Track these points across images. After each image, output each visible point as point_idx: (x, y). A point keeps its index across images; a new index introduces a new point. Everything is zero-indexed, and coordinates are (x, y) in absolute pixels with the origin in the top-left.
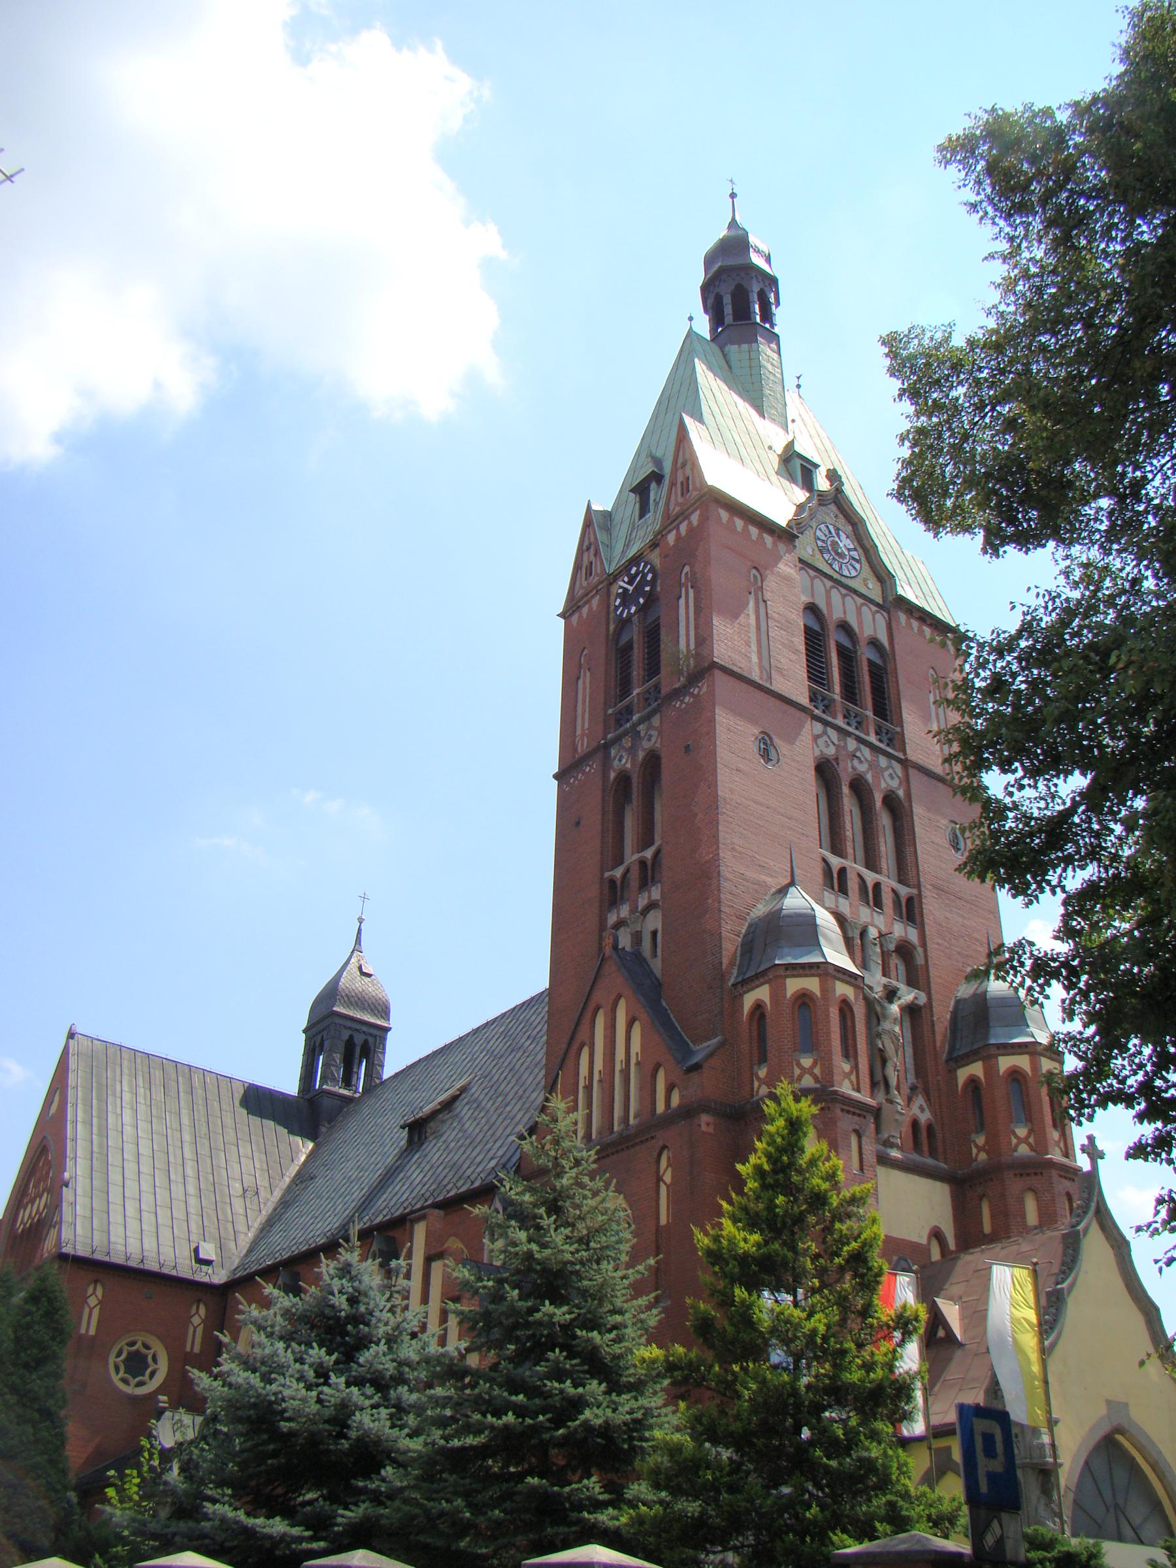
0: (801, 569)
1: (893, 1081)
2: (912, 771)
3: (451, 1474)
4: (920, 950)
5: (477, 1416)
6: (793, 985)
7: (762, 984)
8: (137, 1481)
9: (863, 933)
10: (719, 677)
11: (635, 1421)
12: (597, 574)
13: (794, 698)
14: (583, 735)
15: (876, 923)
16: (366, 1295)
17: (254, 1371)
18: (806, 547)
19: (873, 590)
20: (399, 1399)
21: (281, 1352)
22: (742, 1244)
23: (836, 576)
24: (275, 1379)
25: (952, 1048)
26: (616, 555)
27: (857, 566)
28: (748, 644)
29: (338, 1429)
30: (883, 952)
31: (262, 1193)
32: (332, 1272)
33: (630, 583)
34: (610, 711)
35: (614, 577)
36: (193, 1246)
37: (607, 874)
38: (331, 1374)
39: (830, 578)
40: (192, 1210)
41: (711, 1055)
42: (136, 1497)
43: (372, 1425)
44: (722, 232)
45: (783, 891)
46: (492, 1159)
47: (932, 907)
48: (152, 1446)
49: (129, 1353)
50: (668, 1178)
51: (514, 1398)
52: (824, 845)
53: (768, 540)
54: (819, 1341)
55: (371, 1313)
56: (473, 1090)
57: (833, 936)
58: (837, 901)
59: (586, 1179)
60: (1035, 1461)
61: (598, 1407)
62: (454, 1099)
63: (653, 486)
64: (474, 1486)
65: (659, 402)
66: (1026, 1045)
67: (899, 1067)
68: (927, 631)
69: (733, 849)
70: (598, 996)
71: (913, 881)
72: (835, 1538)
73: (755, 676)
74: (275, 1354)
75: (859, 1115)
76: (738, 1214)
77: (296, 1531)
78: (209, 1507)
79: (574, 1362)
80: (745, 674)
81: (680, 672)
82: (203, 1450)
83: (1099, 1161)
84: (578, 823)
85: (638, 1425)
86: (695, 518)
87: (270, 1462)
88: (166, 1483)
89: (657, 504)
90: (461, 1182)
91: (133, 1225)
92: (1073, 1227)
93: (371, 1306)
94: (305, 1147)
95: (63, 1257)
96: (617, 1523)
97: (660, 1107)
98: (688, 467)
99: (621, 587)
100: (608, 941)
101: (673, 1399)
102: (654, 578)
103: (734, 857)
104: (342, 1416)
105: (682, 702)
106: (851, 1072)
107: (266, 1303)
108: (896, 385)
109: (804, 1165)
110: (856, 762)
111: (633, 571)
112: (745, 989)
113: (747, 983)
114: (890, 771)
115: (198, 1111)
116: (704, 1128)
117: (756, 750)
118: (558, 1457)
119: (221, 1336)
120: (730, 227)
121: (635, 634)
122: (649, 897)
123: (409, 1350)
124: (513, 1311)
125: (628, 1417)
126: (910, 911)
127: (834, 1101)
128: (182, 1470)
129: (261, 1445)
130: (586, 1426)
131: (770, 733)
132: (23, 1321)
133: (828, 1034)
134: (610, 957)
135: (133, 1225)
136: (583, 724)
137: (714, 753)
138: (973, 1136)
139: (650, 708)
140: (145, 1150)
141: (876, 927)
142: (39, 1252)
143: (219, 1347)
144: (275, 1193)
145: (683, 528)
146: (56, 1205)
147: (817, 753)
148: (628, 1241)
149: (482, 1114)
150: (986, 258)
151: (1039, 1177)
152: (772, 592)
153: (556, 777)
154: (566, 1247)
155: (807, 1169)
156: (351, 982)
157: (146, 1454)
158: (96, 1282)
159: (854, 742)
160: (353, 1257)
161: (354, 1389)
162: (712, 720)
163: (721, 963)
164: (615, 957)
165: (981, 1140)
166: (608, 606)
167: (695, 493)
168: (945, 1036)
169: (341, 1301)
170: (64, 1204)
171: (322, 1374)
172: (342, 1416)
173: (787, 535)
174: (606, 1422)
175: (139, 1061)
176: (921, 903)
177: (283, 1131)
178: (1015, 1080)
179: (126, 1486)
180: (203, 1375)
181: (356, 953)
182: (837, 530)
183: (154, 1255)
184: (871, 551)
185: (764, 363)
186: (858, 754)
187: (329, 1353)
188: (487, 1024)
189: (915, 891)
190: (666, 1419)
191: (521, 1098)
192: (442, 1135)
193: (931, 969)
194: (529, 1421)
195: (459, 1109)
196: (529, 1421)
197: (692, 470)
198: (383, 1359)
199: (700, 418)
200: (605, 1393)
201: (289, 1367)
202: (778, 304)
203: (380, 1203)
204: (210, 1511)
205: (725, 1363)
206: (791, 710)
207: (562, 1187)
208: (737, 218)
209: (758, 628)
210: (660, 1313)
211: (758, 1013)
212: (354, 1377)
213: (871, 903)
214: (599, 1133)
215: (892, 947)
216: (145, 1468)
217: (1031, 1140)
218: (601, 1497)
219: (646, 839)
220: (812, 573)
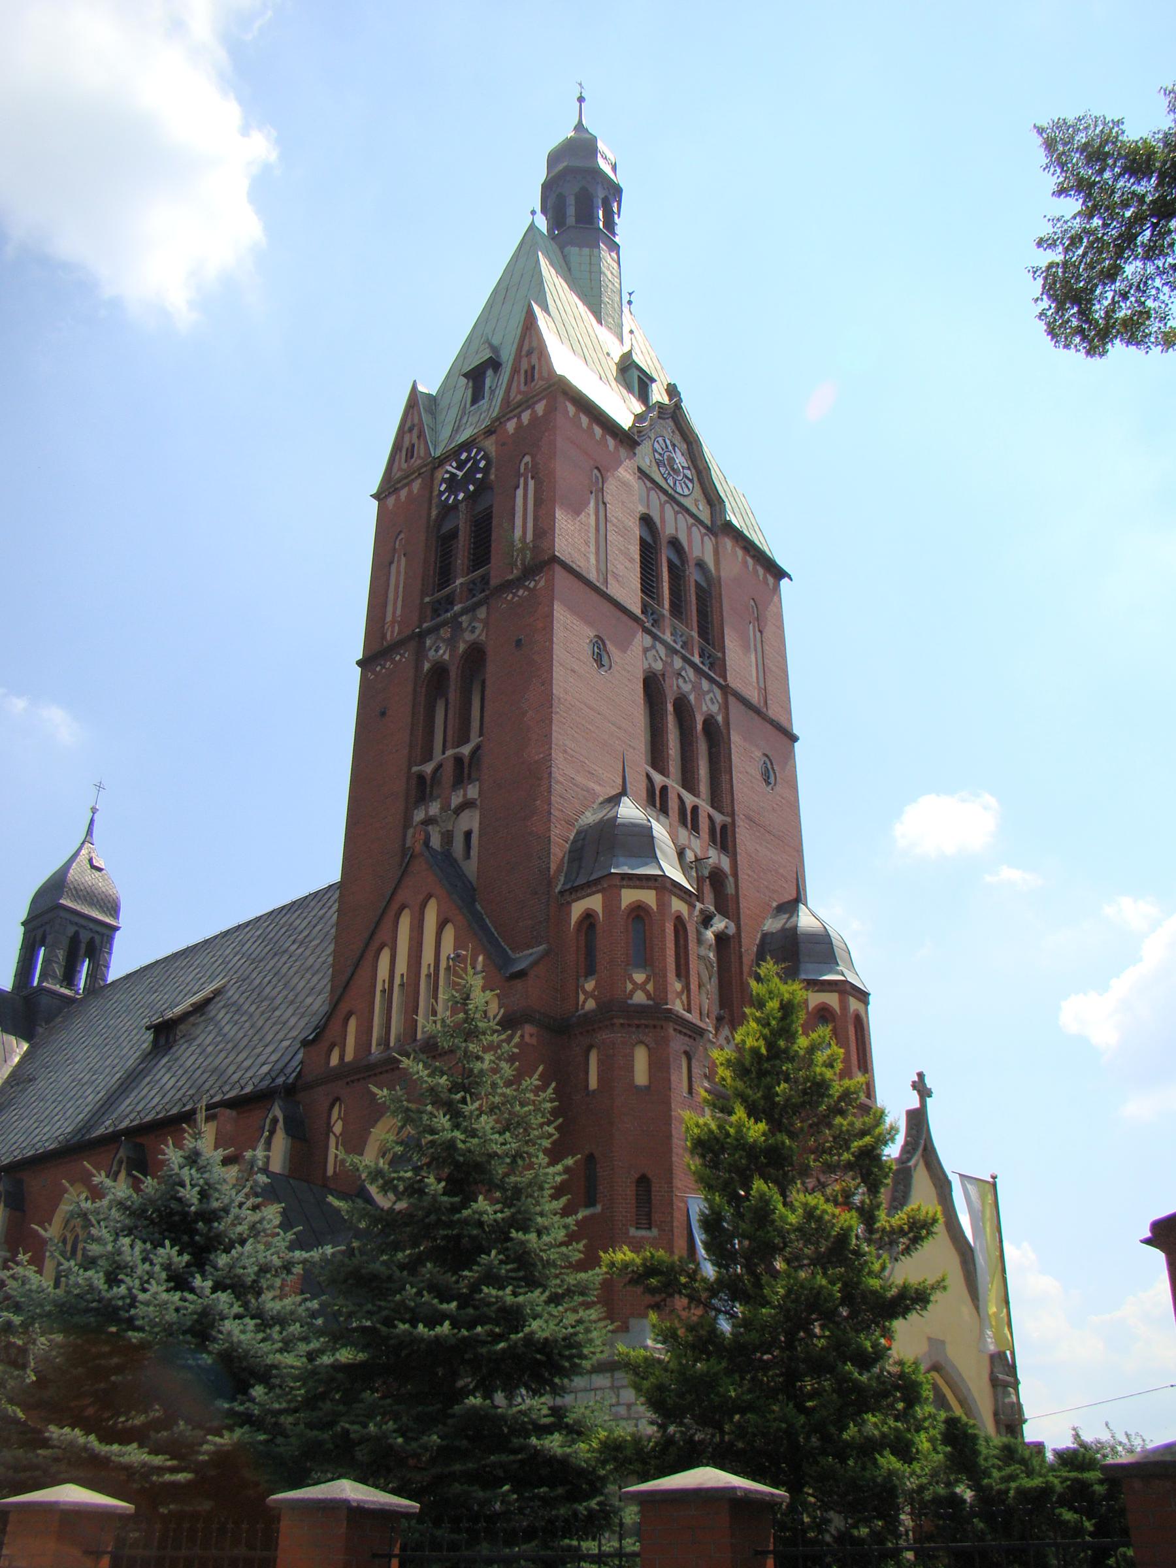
2: (731, 699)
4: (731, 879)
6: (629, 897)
7: (594, 893)
12: (419, 457)
13: (629, 607)
14: (393, 622)
15: (693, 846)
16: (216, 1190)
18: (644, 456)
19: (704, 513)
21: (126, 1249)
23: (670, 491)
26: (443, 440)
27: (690, 485)
28: (587, 543)
30: (698, 877)
33: (459, 468)
34: (427, 599)
35: (441, 461)
37: (415, 769)
39: (665, 492)
41: (535, 964)
45: (615, 800)
46: (264, 1064)
47: (744, 836)
51: (445, 1306)
56: (230, 993)
62: (207, 1001)
63: (490, 372)
65: (495, 292)
66: (836, 982)
69: (565, 751)
71: (728, 809)
72: (881, 1460)
73: (593, 576)
75: (690, 1037)
77: (158, 1460)
79: (509, 1267)
80: (584, 574)
81: (513, 565)
83: (928, 1099)
84: (383, 714)
86: (540, 408)
89: (492, 392)
90: (227, 1088)
92: (903, 1163)
99: (447, 472)
105: (515, 595)
106: (682, 992)
107: (96, 1193)
110: (681, 681)
111: (464, 456)
112: (573, 896)
114: (711, 695)
117: (590, 653)
121: (462, 522)
122: (465, 795)
124: (435, 1208)
126: (723, 838)
127: (668, 1019)
130: (529, 1340)
131: (605, 638)
136: (394, 609)
137: (550, 650)
141: (693, 851)
145: (526, 417)
147: (646, 666)
148: (551, 1135)
149: (244, 1019)
152: (612, 495)
153: (359, 663)
156: (79, 874)
159: (680, 661)
162: (550, 616)
164: (427, 854)
166: (431, 492)
169: (190, 1195)
173: (628, 440)
181: (87, 845)
182: (674, 446)
184: (704, 474)
185: (604, 269)
186: (683, 673)
189: (729, 820)
191: (292, 1002)
192: (195, 1039)
193: (741, 900)
194: (464, 1332)
195: (213, 1013)
196: (464, 1332)
197: (539, 359)
199: (546, 309)
203: (125, 1106)
204: (55, 1436)
206: (625, 618)
208: (584, 122)
209: (597, 530)
214: (398, 1040)
215: (706, 873)
220: (649, 484)
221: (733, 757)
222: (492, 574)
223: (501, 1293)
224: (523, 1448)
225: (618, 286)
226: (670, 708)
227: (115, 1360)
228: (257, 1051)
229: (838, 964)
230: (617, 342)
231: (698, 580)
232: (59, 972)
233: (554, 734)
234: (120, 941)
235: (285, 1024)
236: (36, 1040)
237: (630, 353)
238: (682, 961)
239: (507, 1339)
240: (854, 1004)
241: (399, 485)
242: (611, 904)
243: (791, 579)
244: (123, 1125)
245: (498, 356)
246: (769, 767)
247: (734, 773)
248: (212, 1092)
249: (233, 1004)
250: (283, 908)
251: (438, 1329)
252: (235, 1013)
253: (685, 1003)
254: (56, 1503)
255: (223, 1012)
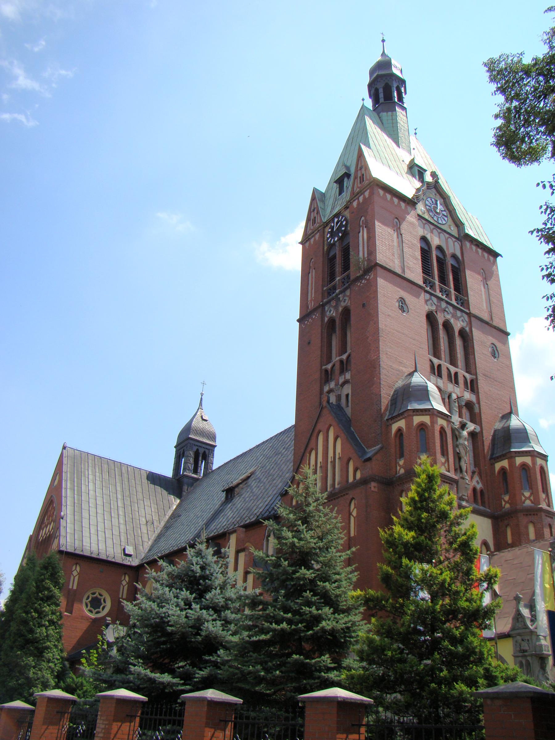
0: (419, 219)
1: (464, 468)
2: (473, 319)
3: (254, 653)
4: (477, 405)
5: (266, 625)
6: (417, 420)
7: (401, 419)
8: (96, 655)
9: (450, 396)
10: (379, 270)
11: (348, 628)
12: (318, 223)
13: (416, 282)
14: (311, 300)
15: (456, 391)
16: (209, 566)
17: (154, 602)
18: (421, 207)
19: (454, 231)
20: (226, 617)
21: (167, 592)
22: (405, 537)
23: (435, 223)
24: (164, 606)
25: (492, 454)
26: (327, 214)
27: (446, 219)
28: (393, 255)
29: (196, 631)
30: (459, 406)
31: (156, 523)
32: (192, 554)
34: (325, 289)
35: (327, 224)
36: (123, 547)
37: (324, 367)
38: (193, 603)
39: (433, 224)
40: (122, 531)
41: (376, 453)
42: (96, 663)
43: (213, 629)
44: (379, 58)
45: (411, 374)
47: (482, 384)
48: (104, 639)
49: (92, 598)
50: (354, 513)
51: (285, 615)
52: (430, 353)
53: (403, 205)
54: (447, 586)
55: (212, 574)
57: (436, 396)
58: (437, 381)
59: (321, 507)
60: (537, 653)
61: (329, 620)
62: (248, 478)
63: (346, 179)
64: (266, 659)
65: (348, 140)
66: (529, 452)
67: (467, 461)
68: (480, 251)
70: (320, 426)
72: (457, 686)
73: (398, 271)
74: (164, 594)
76: (402, 522)
78: (132, 668)
80: (392, 269)
81: (360, 268)
82: (128, 641)
84: (309, 343)
85: (347, 630)
86: (367, 194)
87: (162, 646)
88: (111, 656)
89: (347, 188)
91: (94, 538)
93: (212, 571)
94: (175, 502)
95: (61, 552)
96: (339, 678)
97: (351, 479)
98: (363, 169)
100: (325, 399)
101: (367, 617)
102: (346, 224)
103: (387, 357)
104: (198, 625)
105: (361, 283)
106: (445, 462)
107: (161, 569)
108: (493, 87)
109: (436, 498)
112: (393, 421)
113: (394, 418)
114: (462, 318)
115: (125, 484)
116: (373, 489)
118: (307, 646)
119: (137, 585)
120: (382, 55)
121: (337, 251)
122: (345, 378)
123: (231, 593)
124: (285, 572)
125: (344, 625)
126: (473, 386)
128: (118, 650)
129: (158, 638)
130: (323, 630)
132: (40, 578)
133: (434, 443)
134: (326, 407)
135: (94, 538)
136: (311, 295)
137: (377, 307)
138: (503, 496)
139: (345, 286)
140: (99, 502)
141: (456, 393)
142: (50, 549)
143: (136, 590)
144: (161, 523)
145: (361, 199)
146: (58, 528)
148: (342, 538)
150: (546, 11)
151: (536, 516)
152: (405, 230)
153: (298, 321)
154: (312, 540)
155: (438, 500)
156: (197, 423)
157: (100, 643)
158: (76, 564)
159: (445, 304)
160: (203, 547)
161: (204, 611)
163: (381, 409)
164: (328, 406)
165: (507, 498)
166: (324, 238)
167: (367, 182)
168: (489, 447)
169: (197, 568)
170: (61, 527)
171: (188, 604)
172: (198, 625)
173: (412, 203)
174: (333, 628)
175: (96, 460)
176: (477, 383)
177: (165, 492)
178: (524, 469)
179: (91, 658)
180: (129, 603)
181: (200, 410)
183: (104, 552)
185: (398, 121)
186: (447, 310)
187: (191, 593)
188: (263, 443)
189: (474, 377)
190: (362, 627)
191: (281, 476)
192: (242, 495)
194: (293, 627)
195: (250, 483)
196: (293, 627)
197: (365, 170)
198: (218, 597)
199: (369, 147)
200: (332, 614)
201: (171, 600)
202: (405, 94)
203: (212, 527)
205: (395, 597)
206: (415, 287)
207: (310, 511)
210: (358, 575)
211: (399, 433)
212: (204, 606)
213: (453, 382)
215: (463, 403)
216: (100, 650)
217: (532, 498)
218: (329, 665)
219: (343, 350)
220: (424, 222)
221: (475, 347)
222: (351, 273)
223: (311, 609)
224: (319, 677)
225: (407, 127)
226: (441, 327)
227: (163, 639)
228: (265, 499)
229: (530, 443)
230: (407, 154)
231: (453, 263)
232: (192, 467)
233: (381, 346)
234: (217, 452)
235: (277, 486)
236: (183, 498)
237: (414, 159)
238: (445, 448)
239: (313, 630)
240: (539, 461)
241: (310, 237)
242: (409, 424)
243: (502, 257)
244: (212, 535)
245: (350, 171)
246: (495, 349)
247: (476, 354)
248: (246, 519)
249: (258, 478)
250: (281, 433)
251: (281, 625)
252: (258, 482)
253: (447, 467)
254: (114, 696)
255: (254, 482)
